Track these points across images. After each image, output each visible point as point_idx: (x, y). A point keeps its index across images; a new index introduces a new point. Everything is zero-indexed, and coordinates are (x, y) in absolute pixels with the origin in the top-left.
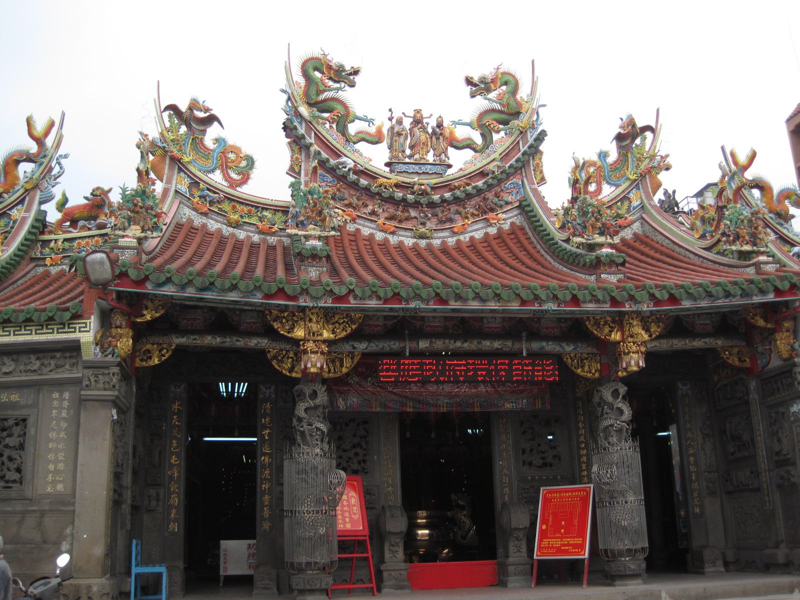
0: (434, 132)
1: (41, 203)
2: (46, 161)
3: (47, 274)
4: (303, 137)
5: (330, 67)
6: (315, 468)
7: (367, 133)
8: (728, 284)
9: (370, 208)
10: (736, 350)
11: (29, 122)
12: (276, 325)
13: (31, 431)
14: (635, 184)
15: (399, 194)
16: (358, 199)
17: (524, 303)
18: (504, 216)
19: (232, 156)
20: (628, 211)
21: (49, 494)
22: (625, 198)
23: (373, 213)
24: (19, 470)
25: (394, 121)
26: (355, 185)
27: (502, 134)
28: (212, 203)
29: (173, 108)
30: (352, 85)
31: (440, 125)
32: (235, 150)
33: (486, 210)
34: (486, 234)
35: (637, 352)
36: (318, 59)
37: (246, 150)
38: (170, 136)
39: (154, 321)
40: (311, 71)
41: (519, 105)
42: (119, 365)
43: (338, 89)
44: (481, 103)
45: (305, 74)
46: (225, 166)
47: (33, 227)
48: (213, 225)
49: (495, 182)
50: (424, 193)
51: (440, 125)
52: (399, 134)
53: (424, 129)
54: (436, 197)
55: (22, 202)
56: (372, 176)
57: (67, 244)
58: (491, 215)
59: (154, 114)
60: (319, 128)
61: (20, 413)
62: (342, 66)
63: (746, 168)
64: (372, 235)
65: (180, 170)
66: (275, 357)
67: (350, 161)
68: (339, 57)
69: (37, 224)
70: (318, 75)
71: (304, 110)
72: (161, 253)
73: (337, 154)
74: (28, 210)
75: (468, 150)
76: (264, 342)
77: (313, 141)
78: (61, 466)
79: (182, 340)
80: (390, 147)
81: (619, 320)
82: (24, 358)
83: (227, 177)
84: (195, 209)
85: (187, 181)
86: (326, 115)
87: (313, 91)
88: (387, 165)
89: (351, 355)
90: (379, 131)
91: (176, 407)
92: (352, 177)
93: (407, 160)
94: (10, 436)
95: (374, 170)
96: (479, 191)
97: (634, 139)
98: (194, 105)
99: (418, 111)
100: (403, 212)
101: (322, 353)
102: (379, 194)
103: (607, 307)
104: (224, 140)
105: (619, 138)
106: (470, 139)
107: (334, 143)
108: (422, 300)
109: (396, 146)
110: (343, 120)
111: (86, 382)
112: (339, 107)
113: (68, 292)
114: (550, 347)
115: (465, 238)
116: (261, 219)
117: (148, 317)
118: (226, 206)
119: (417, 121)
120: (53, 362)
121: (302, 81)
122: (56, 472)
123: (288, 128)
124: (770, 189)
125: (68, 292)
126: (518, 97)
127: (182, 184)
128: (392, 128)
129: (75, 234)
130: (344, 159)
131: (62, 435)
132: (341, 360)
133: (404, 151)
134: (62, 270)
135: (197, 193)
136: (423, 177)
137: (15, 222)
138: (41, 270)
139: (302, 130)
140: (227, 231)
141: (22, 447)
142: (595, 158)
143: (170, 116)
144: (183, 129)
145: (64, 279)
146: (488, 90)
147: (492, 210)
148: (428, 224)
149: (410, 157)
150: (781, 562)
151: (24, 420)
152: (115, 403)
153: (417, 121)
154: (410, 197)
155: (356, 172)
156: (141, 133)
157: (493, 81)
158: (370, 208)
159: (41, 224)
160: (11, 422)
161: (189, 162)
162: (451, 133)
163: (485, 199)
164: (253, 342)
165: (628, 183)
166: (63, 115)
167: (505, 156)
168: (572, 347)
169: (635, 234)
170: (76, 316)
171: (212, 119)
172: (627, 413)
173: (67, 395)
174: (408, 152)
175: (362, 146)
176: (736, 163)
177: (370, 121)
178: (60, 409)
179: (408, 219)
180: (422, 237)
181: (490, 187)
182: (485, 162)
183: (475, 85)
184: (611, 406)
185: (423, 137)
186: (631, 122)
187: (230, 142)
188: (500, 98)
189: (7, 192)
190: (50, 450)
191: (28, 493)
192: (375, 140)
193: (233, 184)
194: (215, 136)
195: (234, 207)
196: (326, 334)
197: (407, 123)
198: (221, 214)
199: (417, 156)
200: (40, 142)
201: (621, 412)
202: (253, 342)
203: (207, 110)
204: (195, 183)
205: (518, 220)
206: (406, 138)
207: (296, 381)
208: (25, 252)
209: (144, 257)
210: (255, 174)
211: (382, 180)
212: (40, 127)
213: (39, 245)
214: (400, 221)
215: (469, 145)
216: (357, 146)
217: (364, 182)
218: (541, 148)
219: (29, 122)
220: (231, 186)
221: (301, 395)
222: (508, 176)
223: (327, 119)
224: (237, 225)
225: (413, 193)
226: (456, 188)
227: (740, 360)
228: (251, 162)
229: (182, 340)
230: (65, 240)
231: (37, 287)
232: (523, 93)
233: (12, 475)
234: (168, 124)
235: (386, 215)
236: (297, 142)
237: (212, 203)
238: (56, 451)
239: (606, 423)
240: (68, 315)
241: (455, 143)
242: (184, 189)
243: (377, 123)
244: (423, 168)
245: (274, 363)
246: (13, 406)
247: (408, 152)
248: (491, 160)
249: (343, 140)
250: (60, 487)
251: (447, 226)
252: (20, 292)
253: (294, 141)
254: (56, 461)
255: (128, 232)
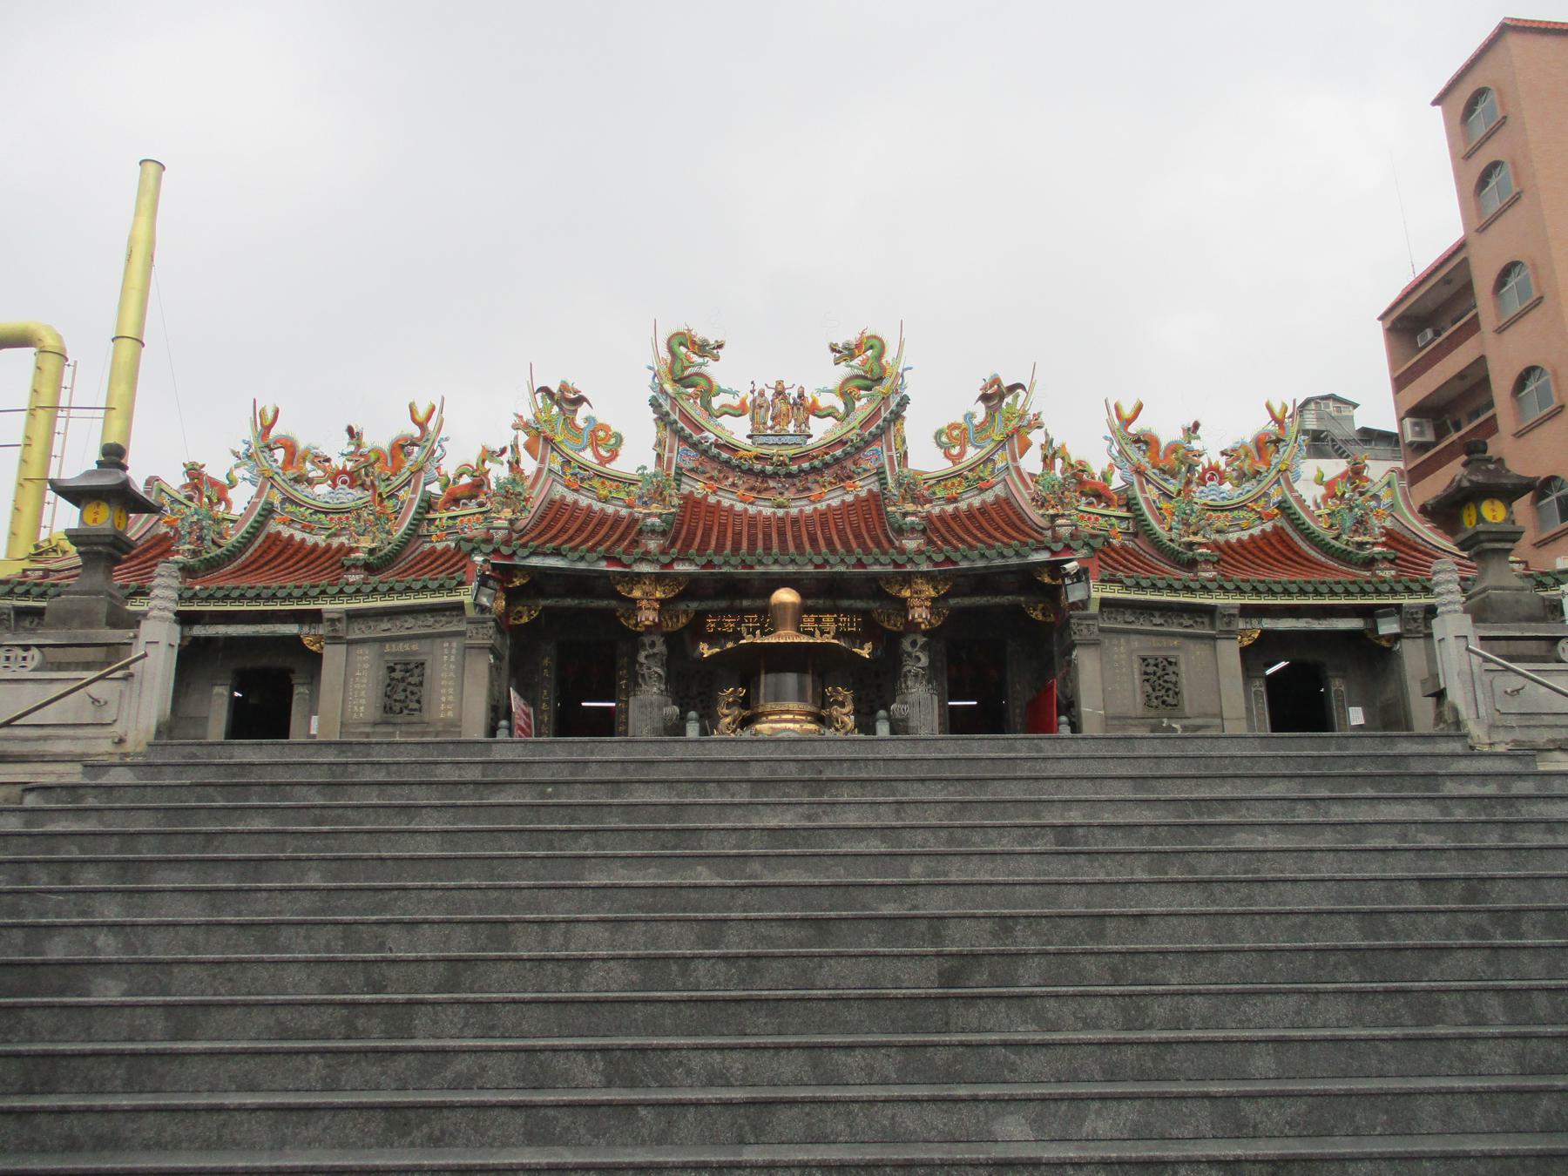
0: (795, 403)
1: (425, 484)
2: (429, 444)
3: (433, 550)
4: (667, 414)
5: (694, 343)
6: (651, 704)
7: (730, 406)
8: (67, 545)
9: (731, 480)
10: (1041, 606)
11: (412, 408)
12: (619, 588)
13: (428, 671)
14: (1001, 445)
15: (758, 466)
16: (720, 472)
17: (817, 566)
18: (861, 483)
19: (601, 434)
20: (992, 472)
21: (442, 720)
22: (987, 460)
23: (733, 485)
24: (418, 702)
25: (756, 394)
26: (715, 458)
27: (864, 401)
28: (583, 480)
29: (545, 390)
30: (716, 359)
31: (801, 396)
32: (606, 428)
33: (845, 478)
34: (843, 502)
35: (921, 606)
36: (681, 334)
37: (614, 428)
38: (543, 417)
39: (522, 586)
40: (675, 347)
41: (884, 369)
42: (494, 620)
43: (701, 365)
44: (843, 371)
45: (671, 350)
46: (595, 443)
47: (420, 507)
48: (584, 501)
49: (853, 450)
50: (783, 464)
51: (801, 396)
52: (761, 407)
53: (785, 398)
54: (794, 468)
55: (408, 484)
56: (732, 448)
57: (450, 522)
58: (849, 482)
59: (528, 396)
60: (684, 404)
61: (419, 658)
62: (705, 340)
63: (1129, 421)
64: (732, 506)
65: (553, 449)
66: (623, 615)
67: (711, 435)
68: (701, 333)
69: (423, 504)
70: (683, 350)
71: (668, 387)
72: (532, 530)
73: (699, 428)
74: (414, 491)
75: (830, 419)
76: (613, 603)
77: (677, 417)
78: (451, 698)
79: (549, 602)
80: (752, 419)
81: (907, 579)
82: (421, 617)
83: (597, 455)
84: (567, 487)
85: (560, 459)
86: (690, 390)
87: (678, 367)
88: (750, 437)
89: (686, 613)
90: (743, 403)
91: (546, 662)
92: (714, 451)
93: (769, 432)
94: (412, 676)
95: (736, 443)
96: (837, 460)
97: (1002, 398)
98: (564, 387)
99: (780, 383)
100: (762, 482)
101: (655, 609)
102: (738, 467)
103: (890, 569)
104: (594, 419)
105: (985, 398)
106: (833, 407)
107: (697, 418)
108: (732, 566)
109: (757, 418)
110: (708, 391)
111: (469, 634)
112: (703, 383)
113: (453, 566)
114: (860, 604)
115: (822, 506)
116: (628, 494)
117: (518, 583)
118: (596, 483)
119: (780, 393)
120: (444, 619)
121: (668, 358)
122: (447, 703)
123: (655, 404)
124: (1157, 442)
125: (453, 566)
126: (884, 361)
127: (555, 463)
128: (754, 400)
129: (457, 511)
130: (706, 434)
131: (452, 674)
132: (678, 617)
133: (765, 423)
134: (448, 546)
135: (569, 471)
136: (784, 447)
137: (403, 503)
138: (427, 546)
139: (667, 407)
140: (597, 506)
141: (421, 684)
142: (960, 420)
143: (542, 397)
144: (556, 409)
145: (450, 554)
146: (852, 357)
147: (850, 478)
148: (787, 494)
149: (772, 428)
150: (790, 680)
151: (423, 664)
152: (492, 649)
153: (780, 393)
154: (769, 468)
155: (718, 446)
156: (516, 415)
157: (858, 346)
158: (731, 480)
159: (428, 504)
160: (412, 666)
161: (561, 442)
162: (814, 402)
163: (843, 468)
164: (604, 603)
165: (993, 445)
166: (443, 399)
167: (865, 424)
168: (878, 604)
169: (997, 497)
170: (461, 583)
171: (580, 400)
172: (924, 661)
173: (454, 645)
174: (770, 423)
175: (726, 421)
176: (1119, 416)
177: (735, 394)
178: (449, 655)
179: (766, 489)
180: (779, 506)
181: (847, 454)
182: (845, 430)
183: (839, 352)
184: (909, 655)
185: (784, 408)
186: (996, 381)
187: (600, 420)
188: (864, 363)
189: (395, 475)
190: (443, 687)
191: (426, 717)
192: (738, 412)
193: (603, 461)
194: (586, 415)
195: (603, 483)
196: (658, 595)
197: (769, 395)
198: (592, 489)
199: (777, 428)
200: (422, 426)
201: (918, 659)
202: (604, 603)
203: (575, 393)
204: (567, 462)
205: (875, 488)
206: (768, 409)
207: (641, 634)
208: (414, 531)
209: (515, 536)
210: (623, 451)
211: (742, 453)
212: (421, 414)
213: (425, 522)
214: (759, 492)
215: (830, 413)
216: (720, 420)
217: (725, 455)
218: (904, 414)
219: (412, 408)
220: (601, 464)
221: (643, 645)
222: (868, 443)
223: (690, 396)
224: (606, 500)
225: (772, 464)
226: (814, 458)
227: (1044, 614)
228: (619, 439)
229: (549, 602)
230: (450, 518)
231: (427, 562)
232: (888, 357)
233: (414, 705)
234: (541, 405)
235: (746, 486)
236: (663, 419)
237: (583, 480)
238: (447, 687)
239: (908, 668)
240: (454, 583)
241: (817, 412)
242: (557, 467)
243: (742, 395)
244: (784, 440)
245: (622, 620)
246: (414, 653)
247: (770, 423)
248: (850, 429)
249: (706, 415)
250: (450, 714)
251: (806, 494)
252: (412, 567)
253: (659, 418)
254: (448, 694)
255: (502, 515)
